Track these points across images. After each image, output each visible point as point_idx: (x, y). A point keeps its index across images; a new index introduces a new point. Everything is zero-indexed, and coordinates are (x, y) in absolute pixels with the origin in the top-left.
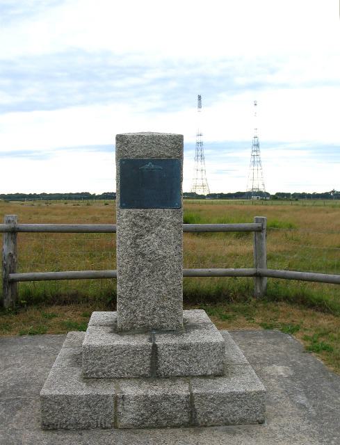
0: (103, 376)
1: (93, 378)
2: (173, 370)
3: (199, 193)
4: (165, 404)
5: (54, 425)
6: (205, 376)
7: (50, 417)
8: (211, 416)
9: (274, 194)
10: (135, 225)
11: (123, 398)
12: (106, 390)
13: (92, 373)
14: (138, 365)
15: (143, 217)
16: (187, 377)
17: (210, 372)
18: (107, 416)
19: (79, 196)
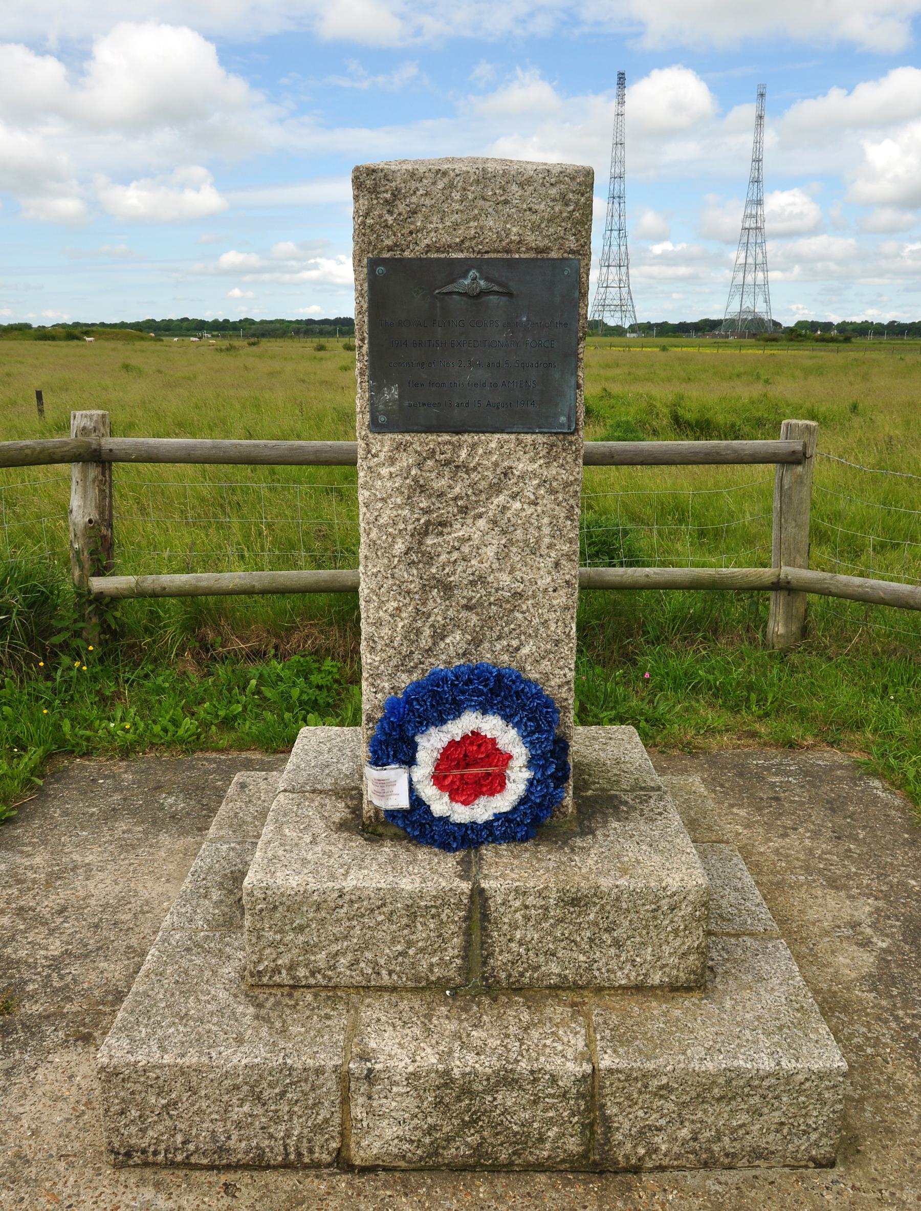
0: (312, 981)
1: (280, 986)
2: (537, 968)
3: (611, 322)
4: (507, 1098)
5: (144, 1152)
6: (639, 989)
7: (133, 1129)
8: (660, 1140)
9: (792, 325)
10: (422, 488)
11: (370, 1077)
12: (315, 1045)
13: (277, 970)
14: (422, 950)
15: (448, 463)
16: (577, 991)
17: (656, 978)
18: (318, 1129)
19: (331, 328)
